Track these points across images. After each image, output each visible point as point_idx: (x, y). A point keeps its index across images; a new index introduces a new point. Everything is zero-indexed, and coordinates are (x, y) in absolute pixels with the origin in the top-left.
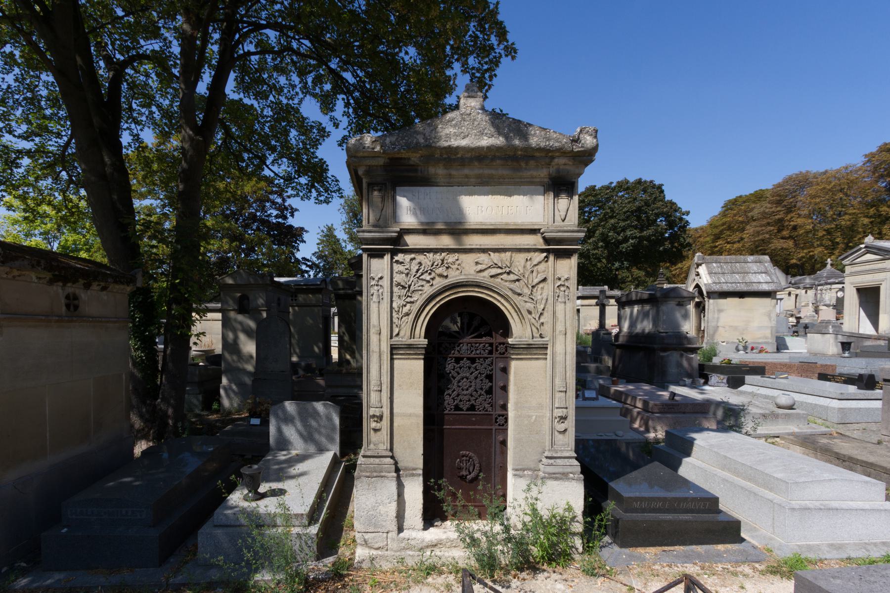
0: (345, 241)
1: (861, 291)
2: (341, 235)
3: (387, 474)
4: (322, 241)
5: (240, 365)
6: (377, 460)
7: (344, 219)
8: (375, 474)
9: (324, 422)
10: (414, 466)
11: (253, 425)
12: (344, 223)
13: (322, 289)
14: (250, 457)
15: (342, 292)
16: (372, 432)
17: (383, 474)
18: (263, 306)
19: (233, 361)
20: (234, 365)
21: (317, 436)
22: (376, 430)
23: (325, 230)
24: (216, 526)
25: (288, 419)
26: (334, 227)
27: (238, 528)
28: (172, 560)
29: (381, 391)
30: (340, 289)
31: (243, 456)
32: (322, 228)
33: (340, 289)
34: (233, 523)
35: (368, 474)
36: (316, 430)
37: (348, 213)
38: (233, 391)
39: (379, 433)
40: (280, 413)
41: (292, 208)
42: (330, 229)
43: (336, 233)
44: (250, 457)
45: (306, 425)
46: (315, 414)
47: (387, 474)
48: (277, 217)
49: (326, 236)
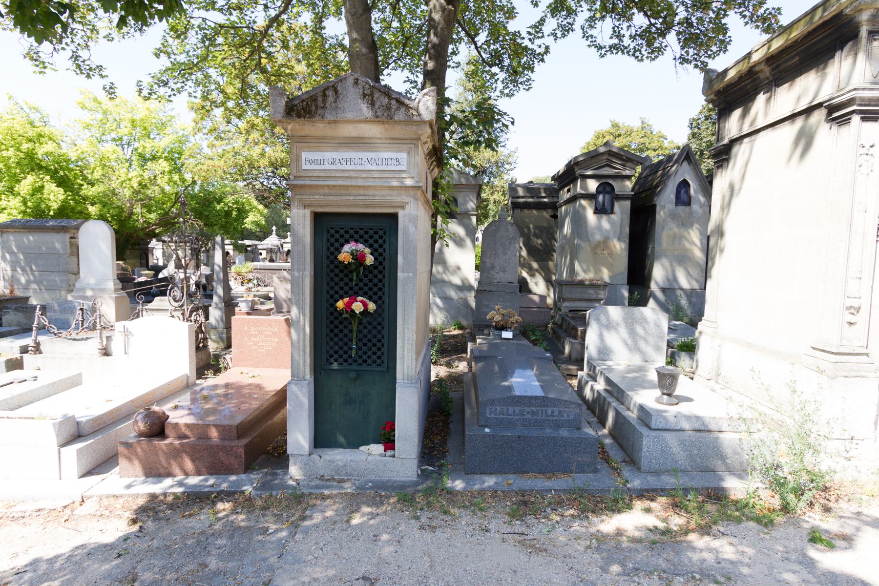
1: (107, 337)
5: (445, 277)
8: (854, 374)
9: (651, 327)
11: (505, 339)
15: (521, 200)
16: (847, 326)
17: (863, 374)
18: (473, 210)
19: (438, 272)
20: (439, 277)
21: (642, 344)
25: (609, 326)
27: (682, 433)
30: (518, 197)
33: (518, 197)
34: (673, 427)
35: (846, 374)
36: (642, 337)
38: (438, 306)
39: (853, 327)
40: (603, 318)
45: (632, 333)
46: (644, 320)
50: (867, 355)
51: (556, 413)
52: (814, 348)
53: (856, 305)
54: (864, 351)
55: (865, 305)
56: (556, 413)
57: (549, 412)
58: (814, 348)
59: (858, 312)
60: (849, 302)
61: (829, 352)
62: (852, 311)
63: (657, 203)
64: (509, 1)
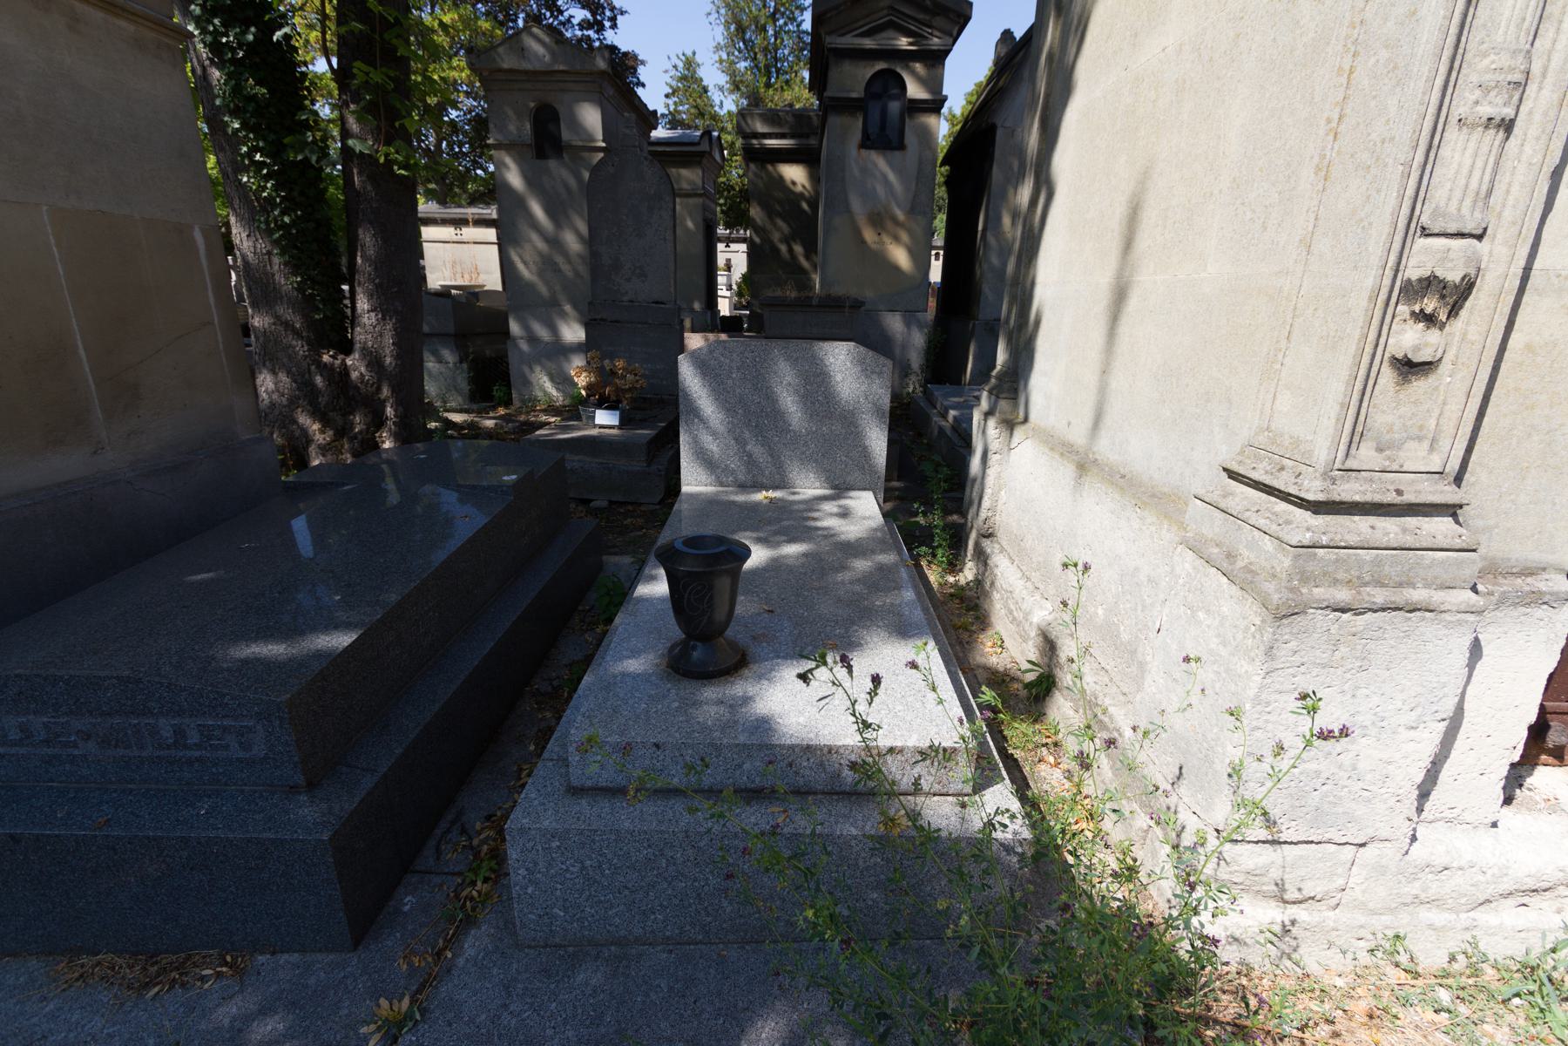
0: (721, 89)
2: (713, 77)
3: (1437, 597)
4: (675, 92)
6: (1389, 529)
7: (720, 39)
8: (1380, 596)
10: (1535, 556)
12: (718, 48)
13: (702, 154)
14: (604, 504)
16: (1388, 376)
17: (1418, 595)
22: (1409, 368)
23: (681, 65)
24: (576, 791)
26: (698, 59)
28: (409, 902)
29: (1507, 126)
31: (586, 502)
32: (675, 60)
35: (1343, 595)
37: (727, 25)
39: (1419, 385)
41: (613, 9)
42: (690, 63)
43: (701, 73)
44: (604, 504)
47: (1437, 597)
48: (584, 25)
49: (683, 78)
50: (1452, 510)
51: (194, 737)
52: (1233, 475)
53: (1454, 276)
54: (1444, 493)
55: (1497, 262)
56: (194, 737)
57: (167, 734)
58: (1233, 475)
59: (1454, 312)
60: (1424, 258)
61: (1285, 497)
62: (1430, 304)
63: (999, 123)
64: (1553, 805)
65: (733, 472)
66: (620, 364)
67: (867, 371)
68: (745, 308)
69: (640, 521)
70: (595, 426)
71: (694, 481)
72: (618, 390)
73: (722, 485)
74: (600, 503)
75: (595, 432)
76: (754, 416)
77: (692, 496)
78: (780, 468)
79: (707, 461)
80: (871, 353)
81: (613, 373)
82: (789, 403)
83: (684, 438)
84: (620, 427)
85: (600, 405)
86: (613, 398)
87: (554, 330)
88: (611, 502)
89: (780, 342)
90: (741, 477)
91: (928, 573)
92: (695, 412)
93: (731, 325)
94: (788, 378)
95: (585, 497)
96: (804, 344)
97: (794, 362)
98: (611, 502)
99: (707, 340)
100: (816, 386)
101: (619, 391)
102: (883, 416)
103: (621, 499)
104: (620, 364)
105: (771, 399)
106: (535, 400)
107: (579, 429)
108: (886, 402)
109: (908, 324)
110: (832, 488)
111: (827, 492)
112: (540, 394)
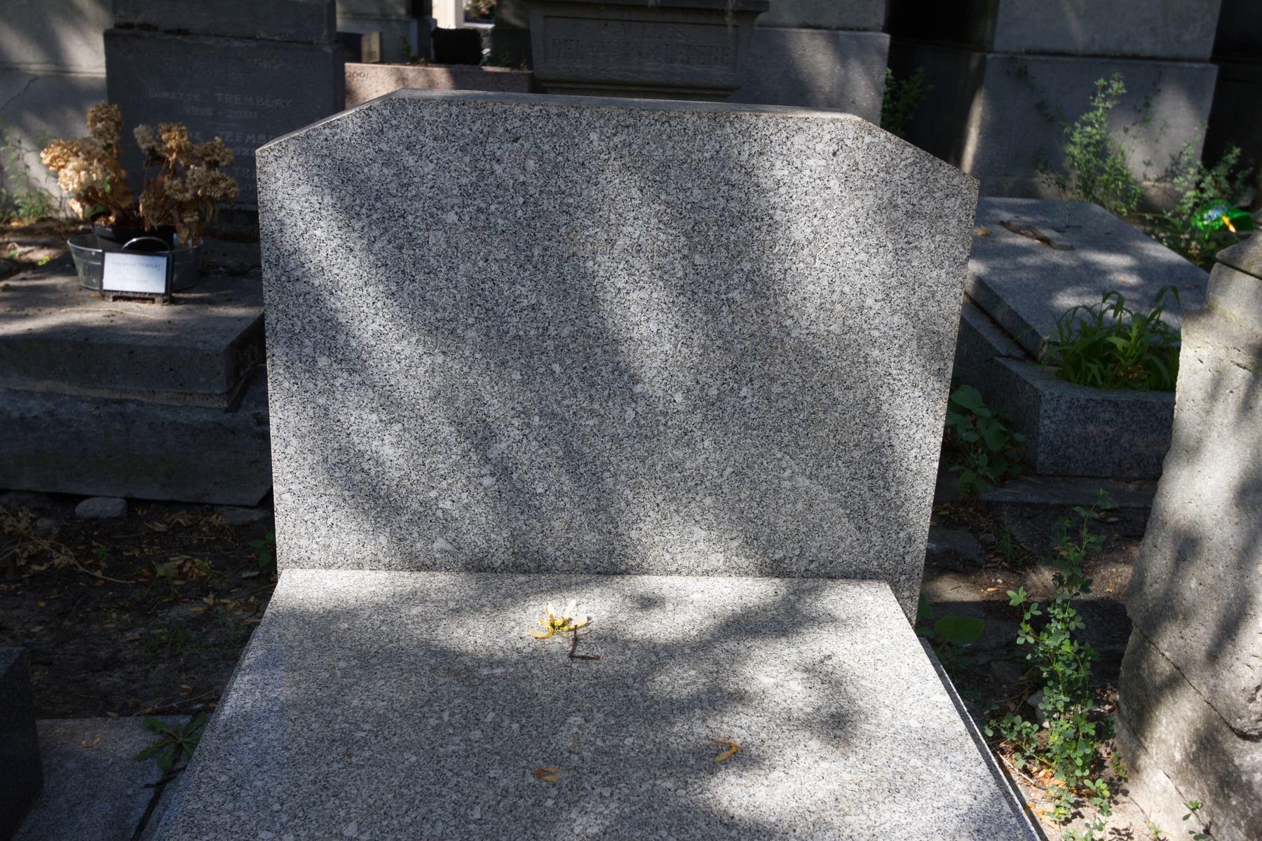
65: (447, 523)
66: (173, 139)
67: (898, 219)
68: (484, 18)
69: (201, 566)
70: (104, 294)
71: (324, 566)
72: (167, 205)
73: (417, 564)
74: (103, 504)
75: (92, 314)
76: (526, 328)
77: (322, 626)
78: (603, 510)
79: (372, 497)
80: (910, 150)
81: (156, 158)
82: (648, 321)
83: (286, 420)
84: (169, 297)
85: (118, 241)
86: (151, 223)
87: (54, 52)
88: (132, 503)
89: (615, 108)
90: (474, 539)
91: (1032, 795)
92: (328, 341)
93: (453, 50)
94: (633, 230)
95: (62, 488)
96: (693, 114)
97: (658, 177)
98: (132, 503)
99: (402, 79)
100: (725, 248)
101: (170, 207)
102: (936, 353)
103: (156, 493)
104: (173, 139)
105: (581, 296)
106: (9, 206)
107: (60, 300)
108: (949, 307)
109: (842, 55)
110: (774, 570)
111: (754, 591)
112: (19, 193)
